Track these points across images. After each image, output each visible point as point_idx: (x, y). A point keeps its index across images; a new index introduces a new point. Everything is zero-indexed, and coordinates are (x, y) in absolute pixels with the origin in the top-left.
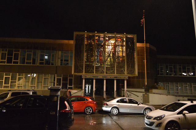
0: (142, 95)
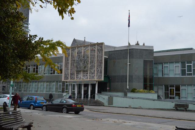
0: (108, 98)
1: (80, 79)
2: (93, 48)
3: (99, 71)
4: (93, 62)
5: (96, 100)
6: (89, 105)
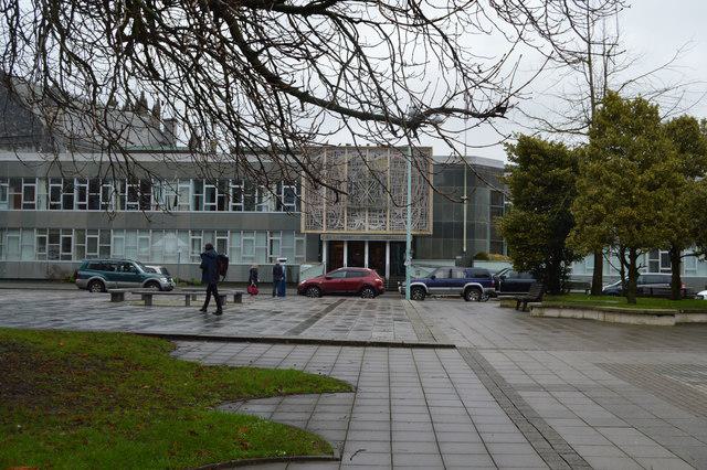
1: (359, 229)
4: (399, 190)
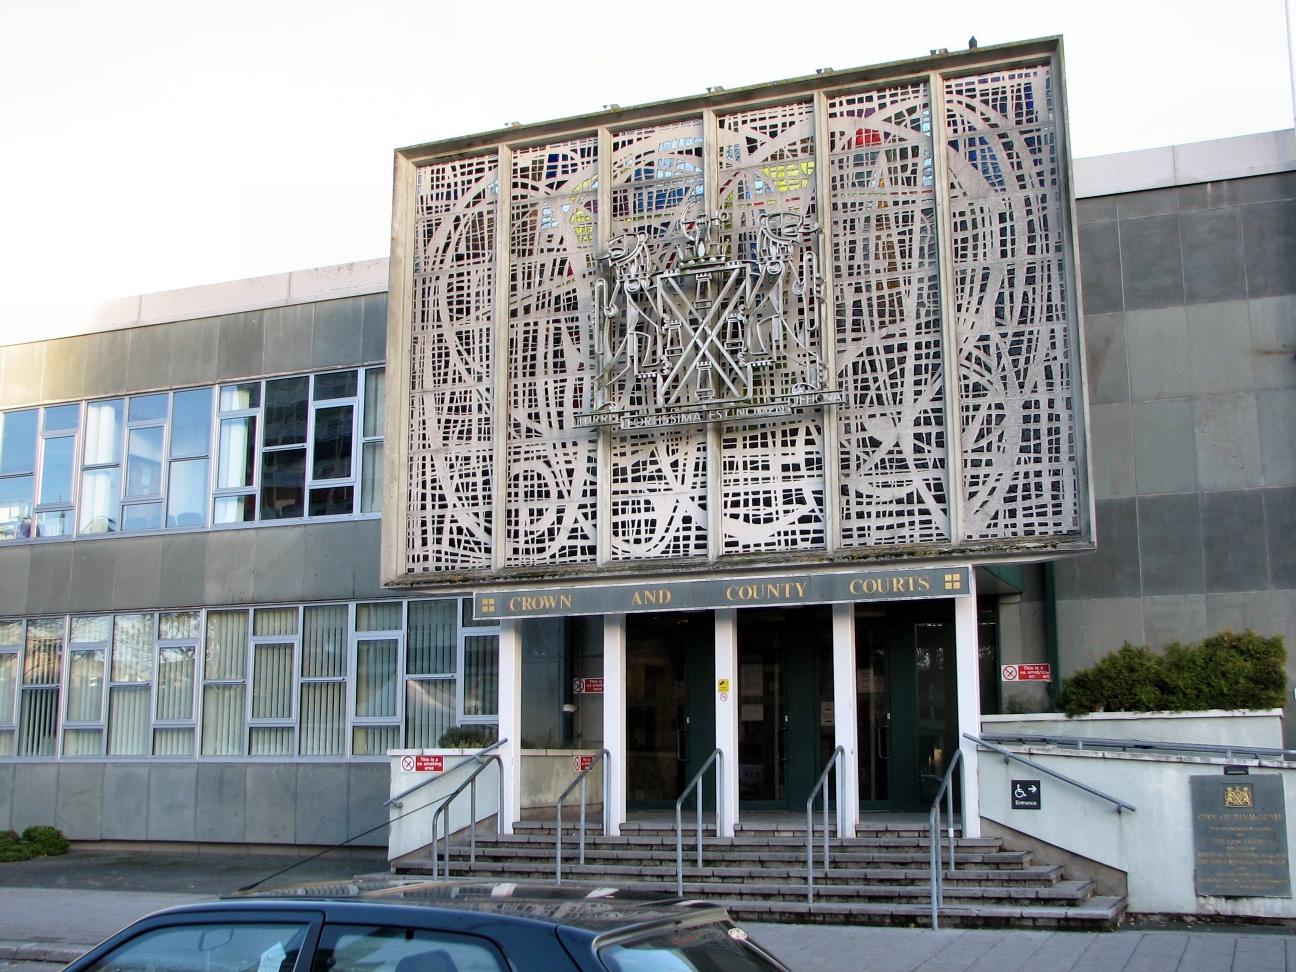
2: (875, 123)
3: (1013, 426)
5: (973, 829)
6: (947, 920)
